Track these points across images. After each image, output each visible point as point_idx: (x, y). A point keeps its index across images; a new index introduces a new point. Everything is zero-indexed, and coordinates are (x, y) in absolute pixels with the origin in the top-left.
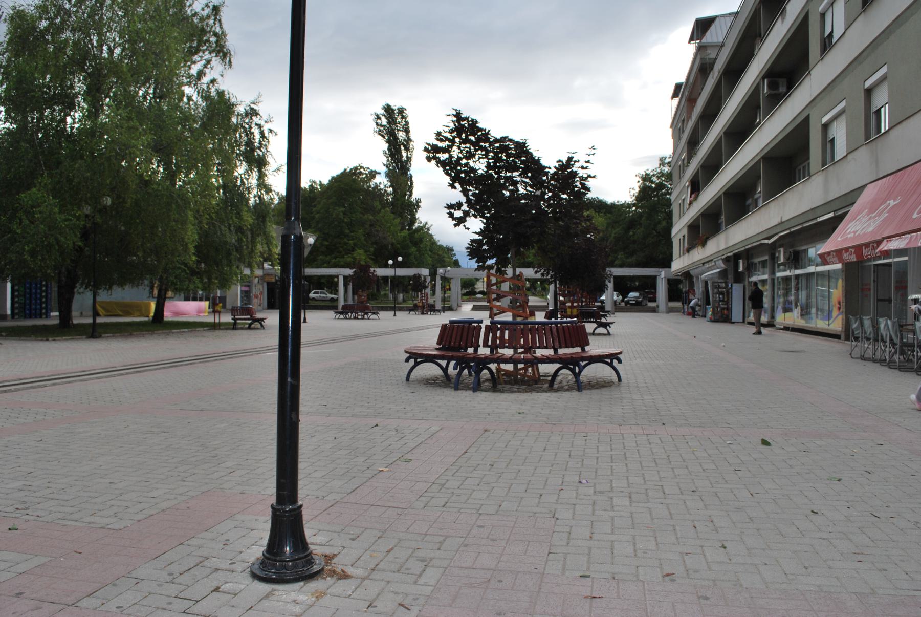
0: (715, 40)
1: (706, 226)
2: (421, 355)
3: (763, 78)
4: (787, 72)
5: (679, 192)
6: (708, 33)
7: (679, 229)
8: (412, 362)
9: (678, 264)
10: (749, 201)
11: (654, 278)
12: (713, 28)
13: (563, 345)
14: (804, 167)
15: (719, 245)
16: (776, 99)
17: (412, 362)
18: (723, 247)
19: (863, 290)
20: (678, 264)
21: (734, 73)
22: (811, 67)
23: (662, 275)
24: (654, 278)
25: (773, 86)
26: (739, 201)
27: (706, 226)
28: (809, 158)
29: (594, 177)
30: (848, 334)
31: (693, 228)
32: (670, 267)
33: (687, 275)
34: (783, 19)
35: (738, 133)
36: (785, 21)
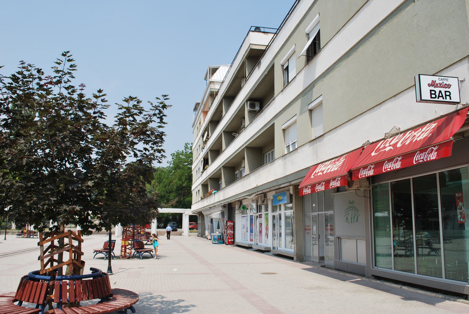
0: (219, 79)
1: (214, 183)
2: (98, 251)
3: (247, 101)
4: (260, 100)
5: (197, 164)
6: (215, 74)
7: (196, 185)
8: (95, 253)
9: (196, 206)
10: (237, 172)
11: (181, 215)
12: (218, 71)
13: (187, 199)
14: (269, 154)
15: (230, 192)
16: (254, 114)
17: (95, 253)
18: (222, 199)
19: (305, 229)
20: (196, 206)
21: (229, 97)
22: (275, 95)
23: (186, 213)
24: (181, 215)
25: (252, 106)
26: (233, 171)
27: (214, 183)
28: (274, 148)
29: (149, 102)
30: (300, 258)
31: (205, 186)
32: (190, 208)
33: (201, 213)
34: (259, 68)
35: (232, 133)
36: (260, 69)
